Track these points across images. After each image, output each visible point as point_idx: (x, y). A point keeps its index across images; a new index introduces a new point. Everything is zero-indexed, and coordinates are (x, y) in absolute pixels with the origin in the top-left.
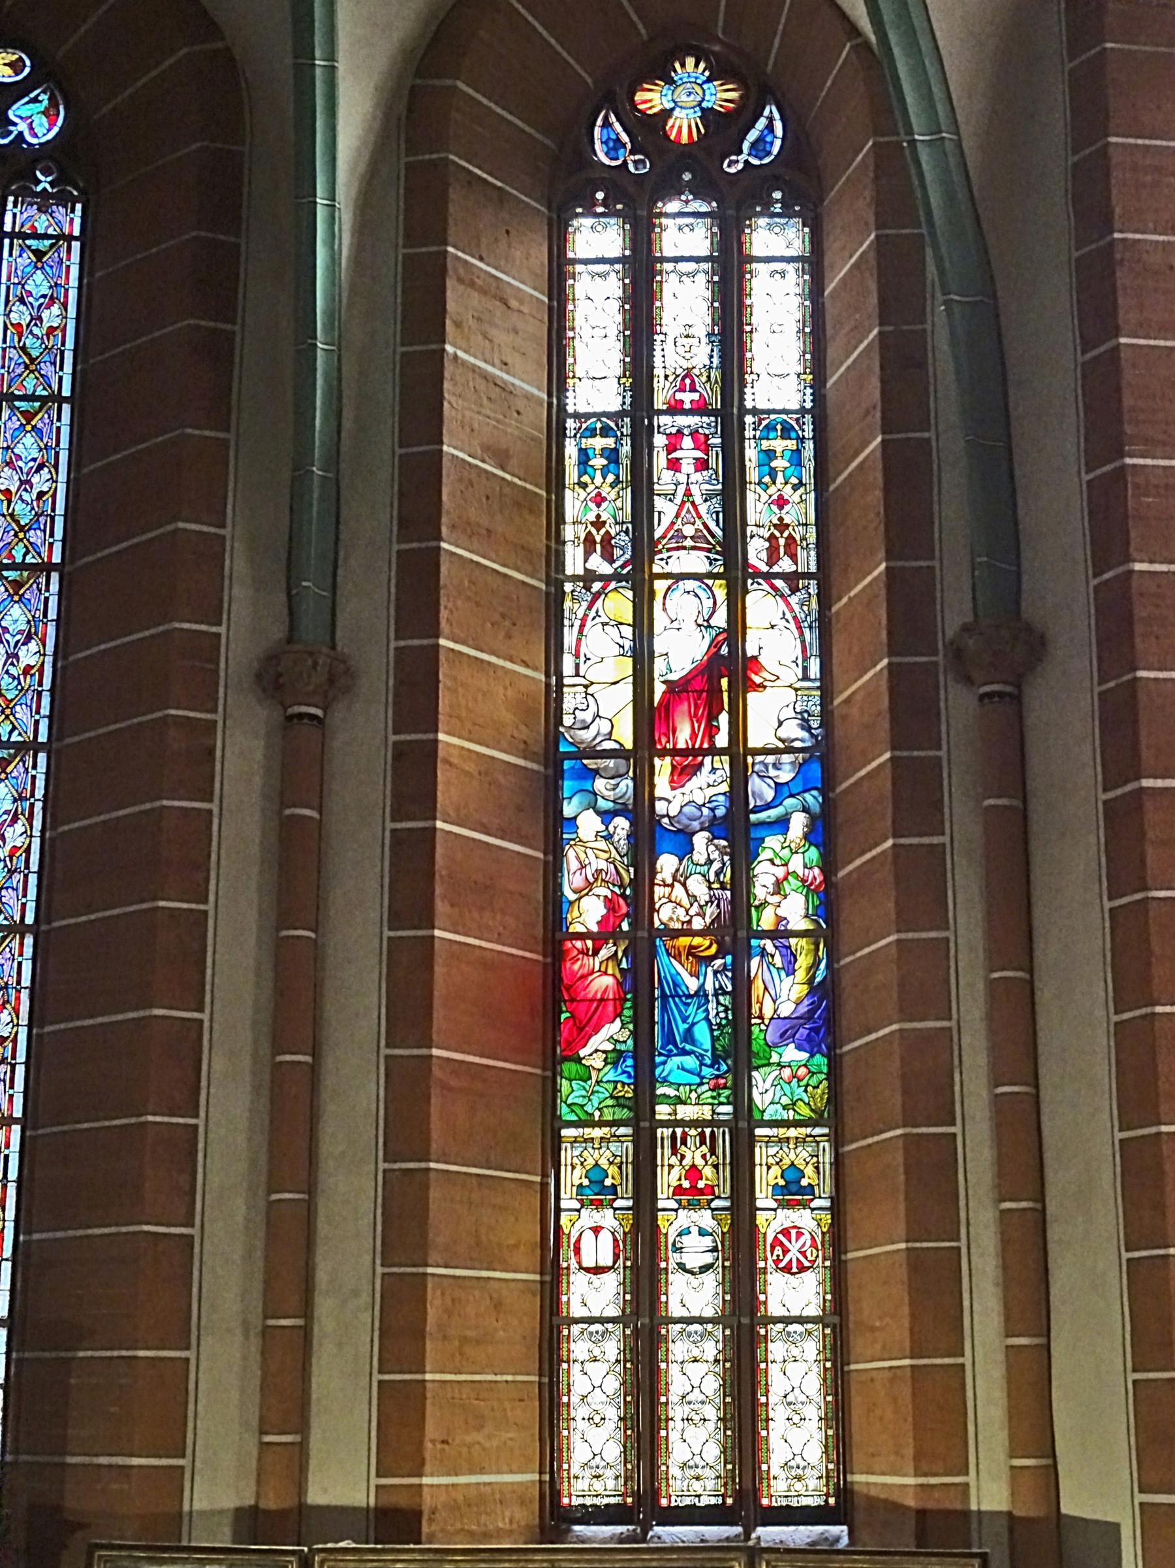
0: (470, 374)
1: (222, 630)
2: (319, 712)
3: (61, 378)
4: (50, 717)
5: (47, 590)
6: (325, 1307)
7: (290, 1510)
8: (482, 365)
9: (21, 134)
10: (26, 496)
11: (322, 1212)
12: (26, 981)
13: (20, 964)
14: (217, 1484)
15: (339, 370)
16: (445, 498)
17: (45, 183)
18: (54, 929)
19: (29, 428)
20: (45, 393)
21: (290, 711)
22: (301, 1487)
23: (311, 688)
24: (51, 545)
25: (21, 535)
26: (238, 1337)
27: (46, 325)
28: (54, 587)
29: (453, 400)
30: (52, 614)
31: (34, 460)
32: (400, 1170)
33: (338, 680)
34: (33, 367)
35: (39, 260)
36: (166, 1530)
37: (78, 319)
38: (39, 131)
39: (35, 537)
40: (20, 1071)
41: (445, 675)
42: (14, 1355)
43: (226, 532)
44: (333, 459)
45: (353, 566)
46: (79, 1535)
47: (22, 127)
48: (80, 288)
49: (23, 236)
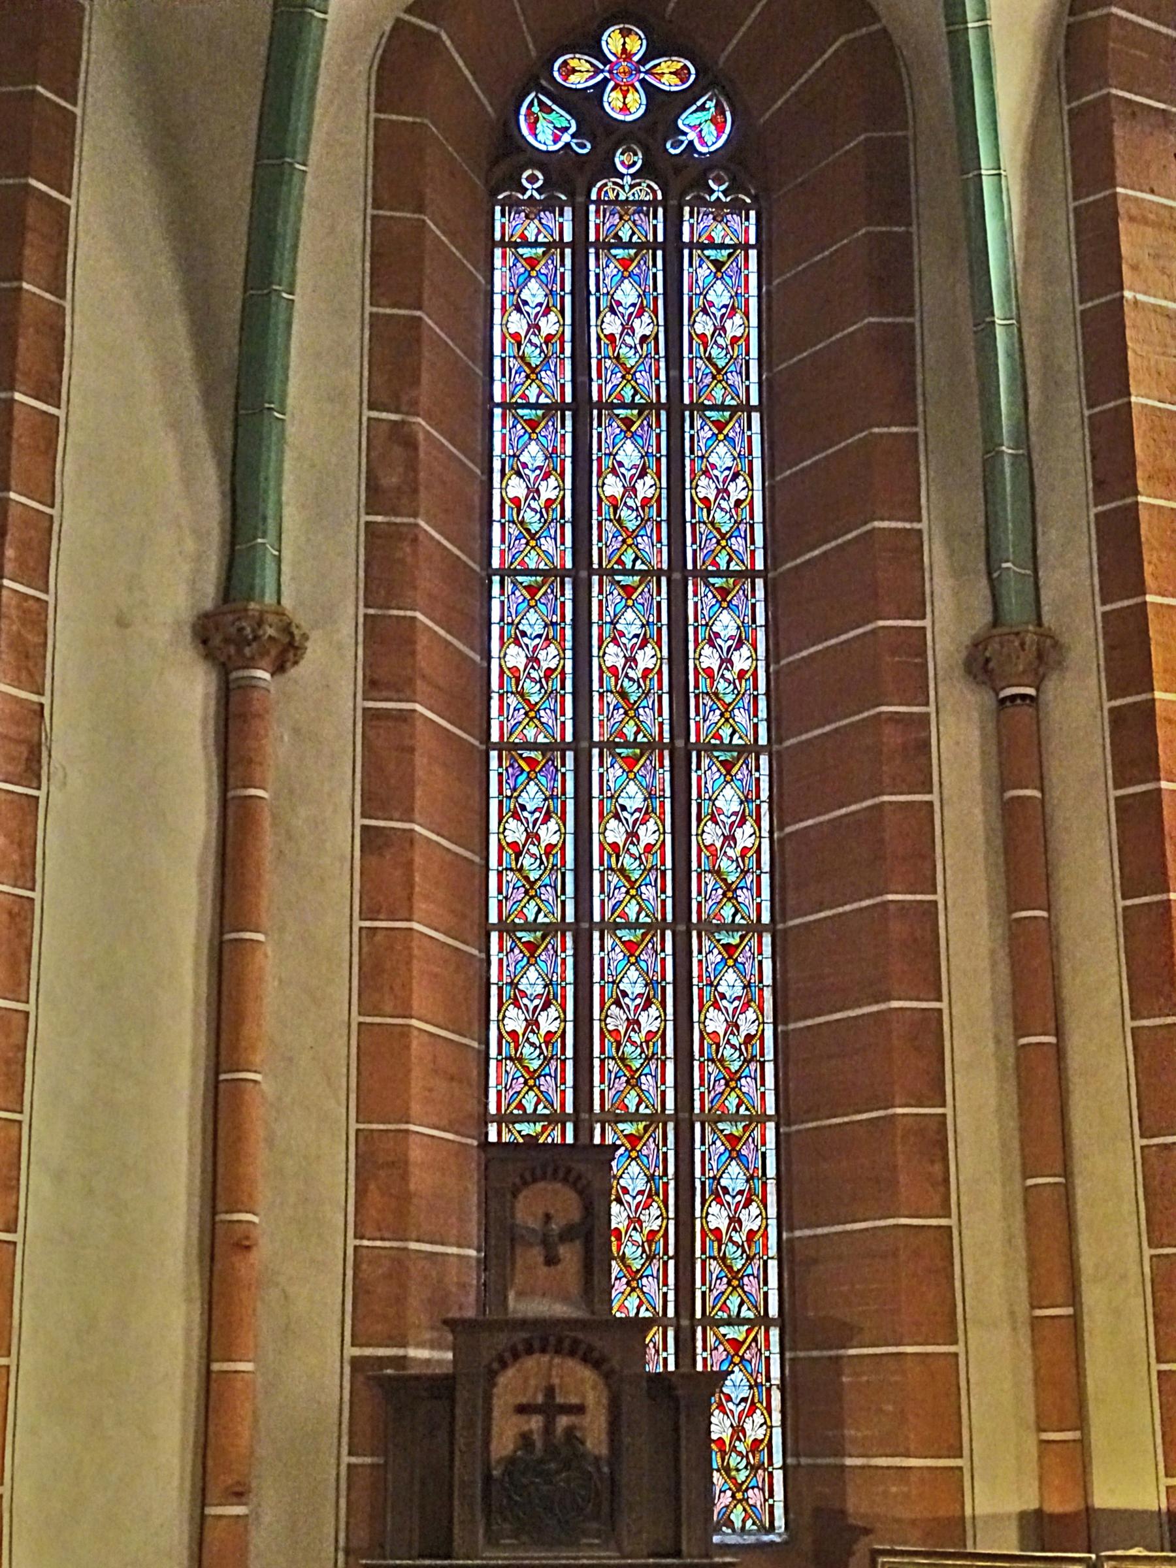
0: (1152, 315)
1: (926, 623)
2: (1031, 691)
3: (748, 388)
4: (768, 720)
5: (754, 596)
6: (1093, 1295)
7: (1076, 1514)
8: (1164, 303)
9: (691, 143)
10: (724, 504)
11: (1079, 1192)
12: (768, 979)
13: (760, 963)
14: (999, 1492)
15: (1021, 342)
16: (1138, 451)
17: (718, 191)
18: (791, 928)
19: (721, 437)
20: (733, 403)
21: (1002, 694)
22: (1086, 1492)
23: (1021, 668)
24: (753, 552)
25: (723, 543)
26: (1006, 1329)
27: (730, 335)
28: (760, 593)
29: (1137, 347)
30: (760, 620)
31: (729, 469)
32: (1157, 1145)
33: (1047, 656)
34: (720, 377)
35: (719, 270)
36: (949, 1531)
37: (760, 327)
38: (709, 139)
39: (737, 544)
40: (769, 1068)
41: (1157, 644)
42: (788, 1355)
43: (923, 525)
44: (1022, 436)
45: (1050, 537)
46: (865, 1540)
47: (692, 136)
48: (759, 296)
49: (703, 247)
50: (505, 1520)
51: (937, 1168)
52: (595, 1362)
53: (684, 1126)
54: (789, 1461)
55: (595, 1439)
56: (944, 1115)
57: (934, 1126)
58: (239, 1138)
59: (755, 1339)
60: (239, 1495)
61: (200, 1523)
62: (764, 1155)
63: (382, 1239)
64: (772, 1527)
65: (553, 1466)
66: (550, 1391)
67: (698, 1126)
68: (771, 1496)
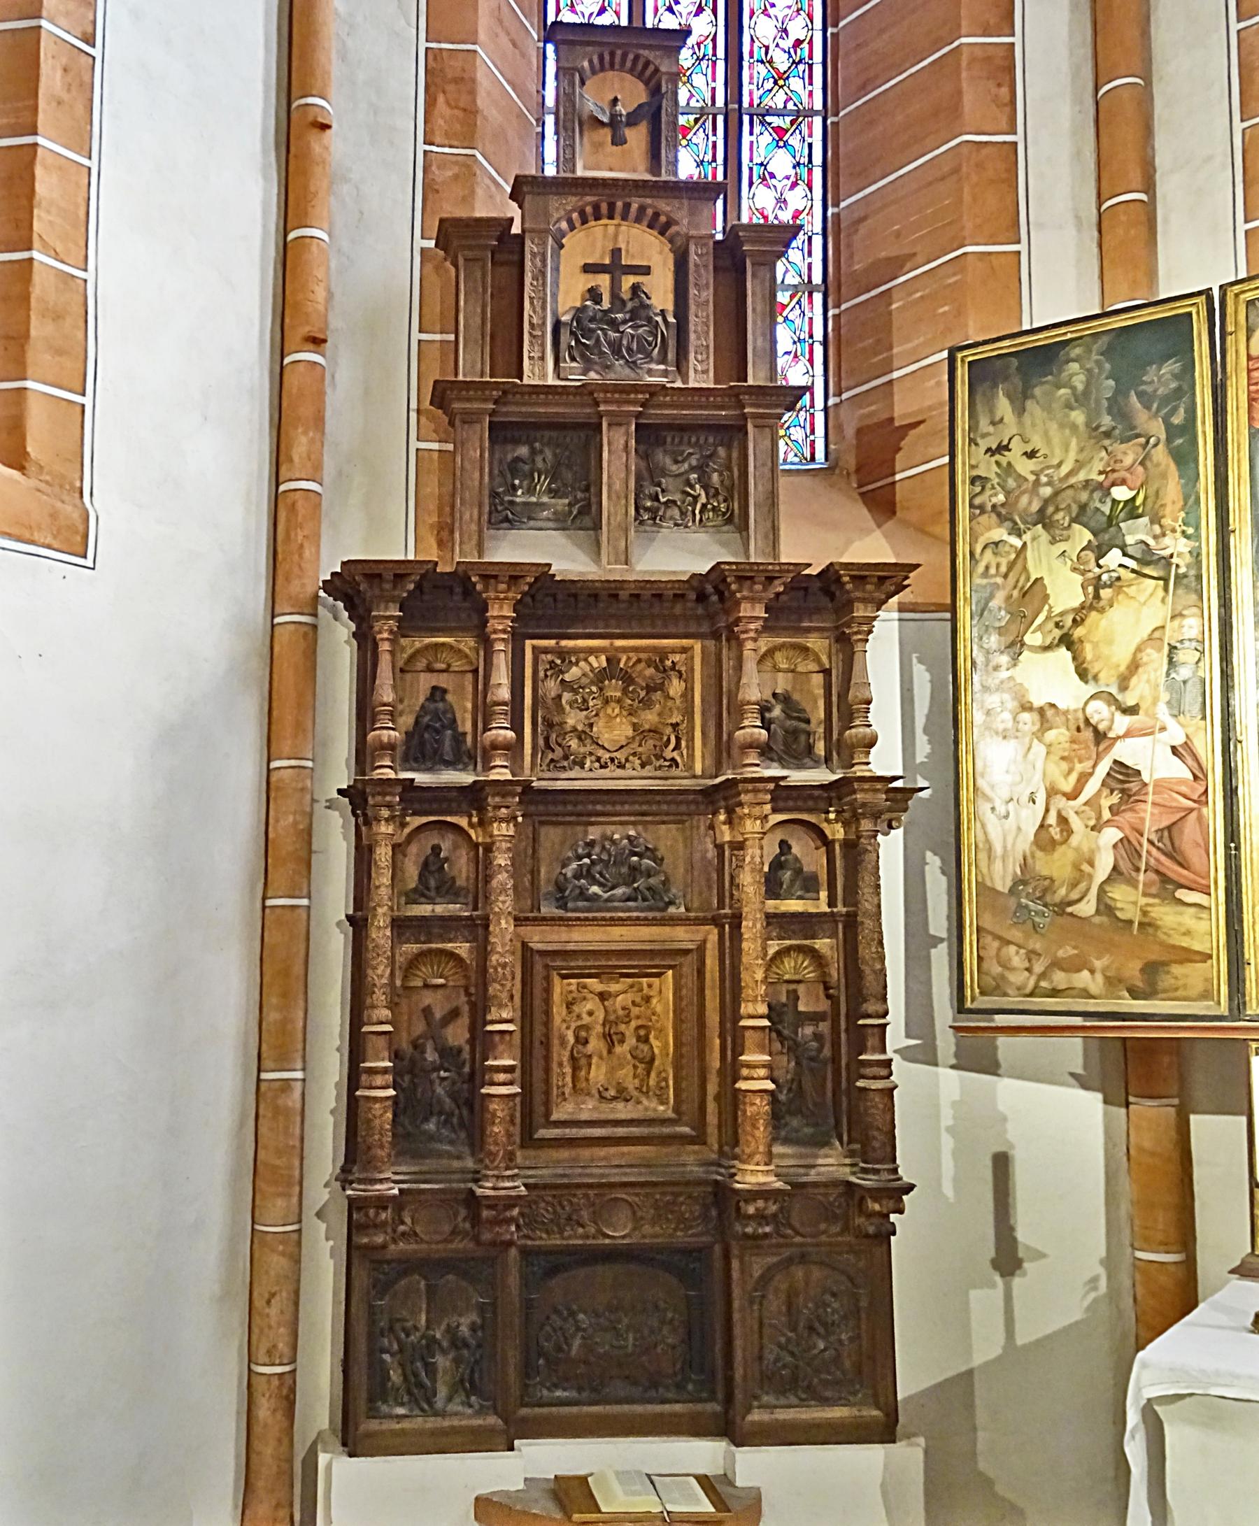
50: (573, 359)
51: (1004, 91)
52: (662, 226)
53: (733, 118)
54: (831, 402)
55: (661, 295)
56: (1013, 44)
57: (1001, 53)
58: (311, 33)
59: (799, 302)
60: (317, 342)
61: (280, 375)
62: (810, 145)
63: (451, 147)
64: (813, 459)
65: (620, 316)
66: (616, 253)
67: (746, 119)
68: (813, 432)
